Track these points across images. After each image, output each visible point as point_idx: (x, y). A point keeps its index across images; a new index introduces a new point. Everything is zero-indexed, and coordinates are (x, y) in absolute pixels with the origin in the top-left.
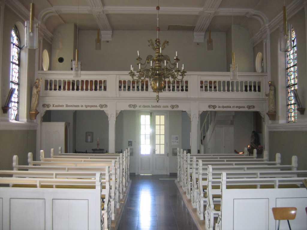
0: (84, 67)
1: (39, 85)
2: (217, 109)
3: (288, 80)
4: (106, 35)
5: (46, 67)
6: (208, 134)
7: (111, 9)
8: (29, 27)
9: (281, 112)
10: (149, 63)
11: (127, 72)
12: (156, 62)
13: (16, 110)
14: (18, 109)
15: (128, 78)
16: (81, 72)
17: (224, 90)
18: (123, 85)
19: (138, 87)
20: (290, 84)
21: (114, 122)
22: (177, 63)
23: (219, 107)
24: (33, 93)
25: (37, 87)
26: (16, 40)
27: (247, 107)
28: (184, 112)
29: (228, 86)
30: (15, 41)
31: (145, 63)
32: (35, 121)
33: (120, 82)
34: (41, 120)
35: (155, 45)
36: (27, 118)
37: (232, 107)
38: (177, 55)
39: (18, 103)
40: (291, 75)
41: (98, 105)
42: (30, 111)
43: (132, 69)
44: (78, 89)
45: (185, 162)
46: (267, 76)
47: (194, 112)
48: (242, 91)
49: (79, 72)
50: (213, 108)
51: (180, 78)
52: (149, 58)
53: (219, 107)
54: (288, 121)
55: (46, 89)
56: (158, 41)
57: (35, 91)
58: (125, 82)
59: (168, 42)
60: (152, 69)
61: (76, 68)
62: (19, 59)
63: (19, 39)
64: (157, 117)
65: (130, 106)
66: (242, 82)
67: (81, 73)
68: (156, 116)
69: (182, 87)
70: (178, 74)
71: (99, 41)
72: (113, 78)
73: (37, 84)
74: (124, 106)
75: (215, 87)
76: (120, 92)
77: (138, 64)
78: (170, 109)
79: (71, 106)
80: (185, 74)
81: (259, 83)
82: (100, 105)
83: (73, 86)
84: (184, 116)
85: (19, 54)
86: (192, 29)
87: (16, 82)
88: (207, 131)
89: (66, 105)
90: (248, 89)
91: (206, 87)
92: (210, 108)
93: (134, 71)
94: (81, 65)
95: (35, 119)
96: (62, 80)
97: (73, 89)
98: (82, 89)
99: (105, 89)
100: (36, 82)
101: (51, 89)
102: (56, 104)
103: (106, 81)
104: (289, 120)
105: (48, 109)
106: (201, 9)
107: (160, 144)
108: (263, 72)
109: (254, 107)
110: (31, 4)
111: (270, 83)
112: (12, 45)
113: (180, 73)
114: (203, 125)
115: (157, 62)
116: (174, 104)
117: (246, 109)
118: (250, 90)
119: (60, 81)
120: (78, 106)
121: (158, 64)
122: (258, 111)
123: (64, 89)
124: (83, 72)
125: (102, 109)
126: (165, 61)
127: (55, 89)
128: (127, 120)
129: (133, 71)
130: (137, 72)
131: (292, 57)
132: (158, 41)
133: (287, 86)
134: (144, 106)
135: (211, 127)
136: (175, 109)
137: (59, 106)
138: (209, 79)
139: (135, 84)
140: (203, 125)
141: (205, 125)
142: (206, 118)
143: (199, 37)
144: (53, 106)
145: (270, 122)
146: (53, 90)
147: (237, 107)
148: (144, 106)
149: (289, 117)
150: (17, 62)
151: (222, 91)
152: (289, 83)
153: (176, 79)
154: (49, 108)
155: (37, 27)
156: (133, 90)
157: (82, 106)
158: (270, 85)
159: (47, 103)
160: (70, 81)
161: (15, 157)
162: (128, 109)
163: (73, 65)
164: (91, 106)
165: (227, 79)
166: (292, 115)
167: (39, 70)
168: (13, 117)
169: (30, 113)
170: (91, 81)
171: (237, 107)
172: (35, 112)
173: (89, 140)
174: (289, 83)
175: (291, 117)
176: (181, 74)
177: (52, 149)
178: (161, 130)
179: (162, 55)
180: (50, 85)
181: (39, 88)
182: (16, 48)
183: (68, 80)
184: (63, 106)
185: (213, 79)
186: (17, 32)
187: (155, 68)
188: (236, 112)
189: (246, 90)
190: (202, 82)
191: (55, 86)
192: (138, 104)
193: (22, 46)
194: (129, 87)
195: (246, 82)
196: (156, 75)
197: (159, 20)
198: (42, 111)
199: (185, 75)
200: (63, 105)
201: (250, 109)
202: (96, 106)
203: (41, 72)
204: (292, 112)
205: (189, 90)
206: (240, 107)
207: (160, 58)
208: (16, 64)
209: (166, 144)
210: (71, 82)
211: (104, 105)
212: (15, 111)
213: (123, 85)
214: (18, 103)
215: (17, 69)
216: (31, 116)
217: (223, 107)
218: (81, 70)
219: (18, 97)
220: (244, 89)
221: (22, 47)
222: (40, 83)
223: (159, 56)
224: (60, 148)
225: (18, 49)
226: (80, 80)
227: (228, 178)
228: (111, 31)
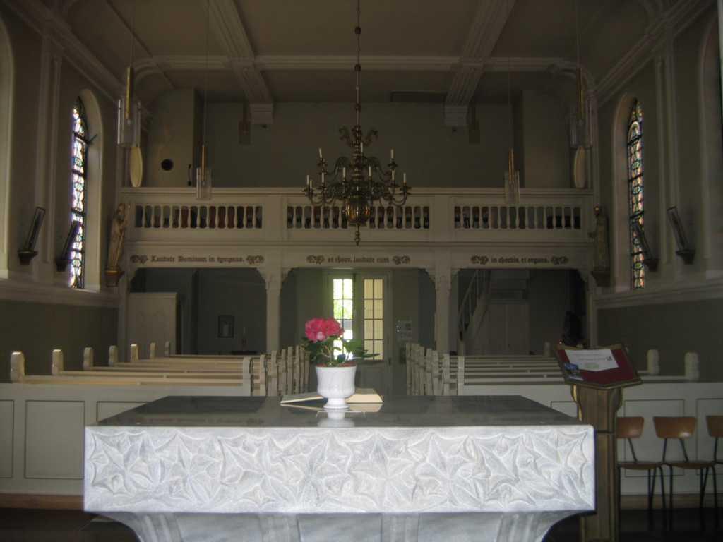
0: (220, 180)
1: (124, 216)
2: (489, 265)
3: (633, 204)
4: (261, 113)
5: (136, 180)
6: (475, 319)
7: (270, 61)
8: (125, 110)
9: (619, 271)
10: (340, 171)
11: (300, 190)
12: (353, 169)
13: (78, 267)
14: (83, 265)
15: (304, 202)
16: (211, 191)
17: (513, 226)
18: (295, 217)
19: (326, 220)
20: (636, 212)
21: (278, 293)
22: (393, 173)
23: (494, 260)
24: (112, 232)
25: (120, 221)
26: (79, 126)
27: (552, 260)
28: (422, 271)
29: (519, 218)
30: (78, 128)
31: (335, 171)
32: (115, 289)
33: (290, 210)
34: (128, 289)
35: (353, 138)
36: (101, 283)
37: (520, 260)
38: (392, 157)
39: (82, 252)
40: (638, 193)
41: (244, 257)
42: (106, 269)
43: (309, 182)
44: (203, 225)
45: (436, 381)
46: (592, 195)
47: (444, 270)
48: (540, 226)
49: (208, 190)
50: (482, 263)
51: (399, 199)
52: (341, 162)
53: (494, 260)
54: (634, 286)
55: (138, 224)
56: (357, 131)
57: (116, 228)
58: (299, 210)
59: (375, 133)
60: (345, 182)
61: (202, 182)
62: (85, 165)
63: (85, 125)
64: (368, 283)
65: (309, 258)
66: (540, 209)
67: (213, 192)
68: (366, 281)
69: (417, 219)
70: (394, 191)
71: (245, 126)
72: (273, 202)
73: (120, 213)
74: (298, 260)
75: (485, 220)
76: (290, 229)
77: (320, 174)
78: (392, 264)
79: (190, 259)
80: (409, 191)
81: (577, 210)
82: (249, 257)
83: (192, 217)
84: (423, 279)
85: (85, 153)
86: (438, 99)
87: (80, 209)
88: (473, 312)
89: (180, 257)
90: (554, 222)
91: (466, 219)
92: (474, 263)
93: (313, 186)
94: (212, 176)
95: (117, 284)
96: (171, 207)
97: (193, 225)
98: (212, 225)
99: (259, 225)
100: (118, 211)
101: (148, 225)
102: (159, 255)
103: (261, 208)
104: (636, 285)
105: (141, 266)
106: (455, 60)
107: (373, 340)
108: (586, 187)
109: (566, 260)
110: (129, 70)
111: (597, 209)
112: (73, 135)
113: (398, 191)
114: (465, 300)
115: (356, 170)
116: (255, 254)
117: (550, 265)
118: (559, 225)
119: (166, 208)
120: (204, 260)
121: (359, 172)
122: (575, 267)
123: (175, 225)
124: (215, 190)
125: (253, 266)
126: (370, 168)
127: (157, 226)
128: (306, 291)
129: (311, 187)
130: (320, 189)
131: (638, 155)
132: (357, 131)
133: (631, 215)
134: (340, 260)
135: (480, 304)
136: (403, 265)
137: (164, 259)
138: (471, 202)
139: (320, 214)
140: (465, 300)
141: (468, 300)
142: (471, 284)
143: (456, 115)
144: (153, 260)
145: (599, 290)
146: (152, 228)
147: (530, 260)
148: (340, 260)
149: (634, 279)
150: (82, 171)
151: (499, 228)
152: (634, 210)
153: (394, 202)
154: (143, 263)
155: (139, 110)
156: (317, 226)
157: (212, 260)
158: (598, 214)
159: (140, 254)
160: (186, 207)
161: (87, 351)
162: (306, 264)
163: (78, 181)
164: (231, 260)
165: (500, 203)
166: (641, 276)
167: (123, 185)
168: (73, 281)
169: (106, 274)
170: (231, 209)
171: (530, 260)
172: (117, 270)
173: (226, 332)
174: (634, 210)
175: (638, 278)
176: (402, 192)
177: (153, 345)
178: (375, 309)
179: (365, 155)
180: (144, 217)
181: (124, 223)
182: (79, 142)
183: (183, 207)
184: (174, 259)
185: (480, 202)
186: (82, 110)
187: (352, 180)
188: (534, 272)
189: (550, 226)
190: (457, 210)
191: (157, 219)
192: (327, 255)
193: (90, 138)
194: (308, 221)
195: (550, 209)
196: (355, 193)
197: (360, 91)
198: (131, 269)
199: (409, 194)
200: (173, 256)
201: (558, 263)
202: (241, 260)
203: (126, 189)
204: (640, 269)
205: (431, 227)
206: (536, 261)
207: (361, 163)
208: (80, 175)
209: (386, 340)
210: (189, 210)
211: (256, 258)
212: (77, 269)
213: (295, 217)
214: (82, 252)
215: (81, 184)
216: (108, 279)
217: (502, 260)
218: (214, 185)
219: (82, 241)
220: (545, 223)
221: (92, 139)
222: (128, 213)
223: (359, 158)
224: (167, 344)
225: (82, 143)
226: (208, 207)
227: (468, 363)
228: (272, 105)
